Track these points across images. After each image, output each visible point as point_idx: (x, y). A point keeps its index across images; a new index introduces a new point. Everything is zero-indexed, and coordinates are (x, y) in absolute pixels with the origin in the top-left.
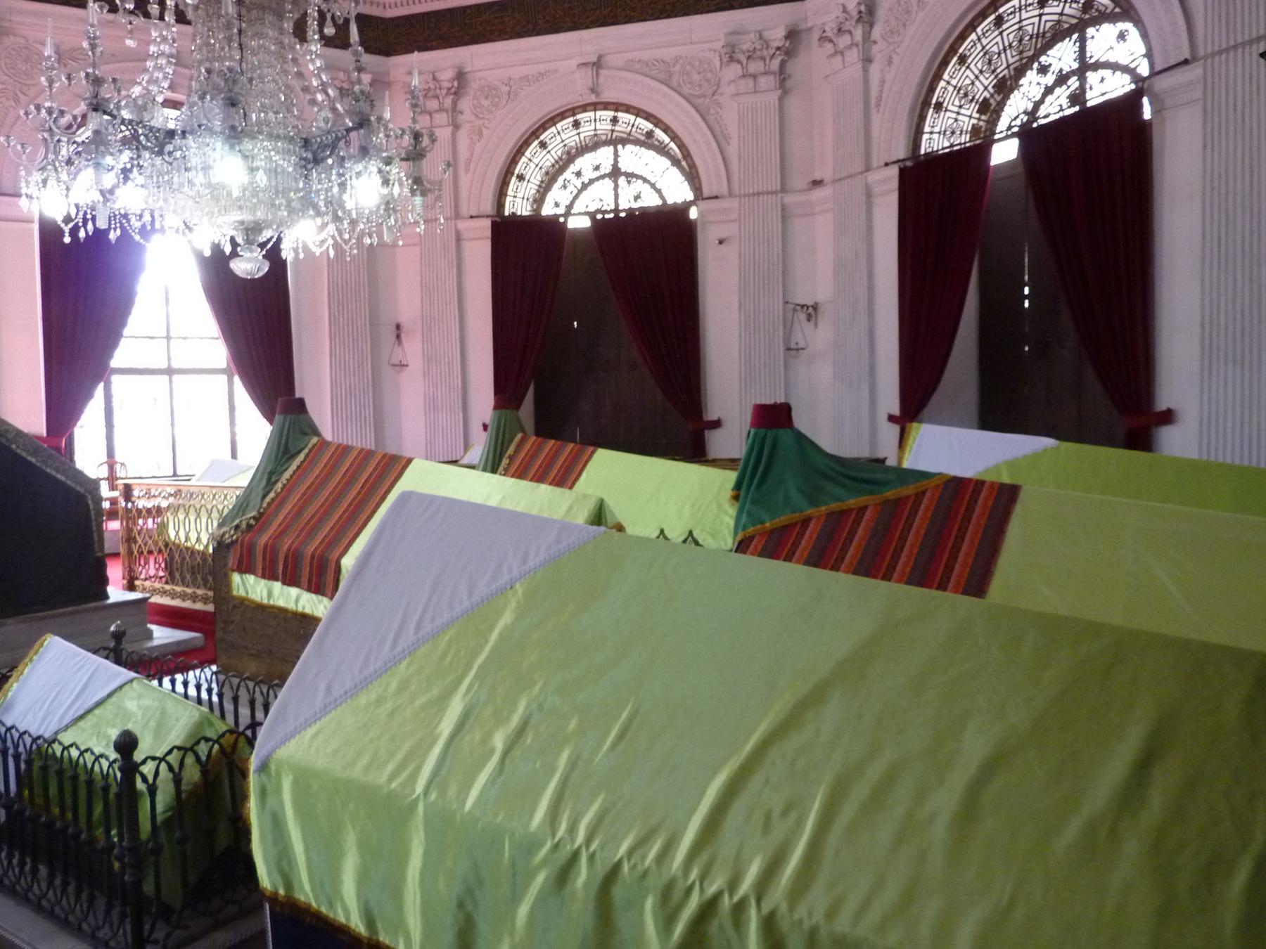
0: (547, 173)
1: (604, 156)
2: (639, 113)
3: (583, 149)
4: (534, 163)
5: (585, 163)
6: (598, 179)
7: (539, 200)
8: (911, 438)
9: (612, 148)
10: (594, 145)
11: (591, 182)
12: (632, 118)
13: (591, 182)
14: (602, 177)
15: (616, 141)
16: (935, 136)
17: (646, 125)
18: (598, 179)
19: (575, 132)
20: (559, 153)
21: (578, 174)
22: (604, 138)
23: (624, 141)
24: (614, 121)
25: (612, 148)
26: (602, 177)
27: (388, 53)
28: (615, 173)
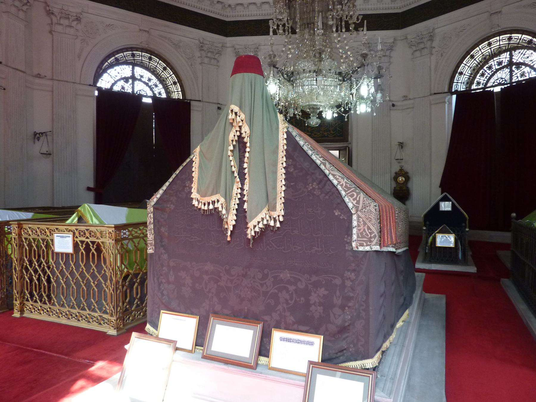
0: (474, 70)
1: (505, 58)
2: (523, 32)
3: (493, 56)
4: (466, 67)
5: (493, 63)
6: (500, 69)
7: (470, 82)
8: (243, 371)
9: (131, 66)
10: (499, 52)
11: (497, 70)
12: (520, 35)
13: (497, 70)
14: (503, 67)
15: (511, 49)
16: (459, 84)
17: (528, 38)
18: (500, 69)
19: (132, 58)
20: (163, 76)
21: (156, 86)
22: (504, 48)
23: (515, 49)
24: (510, 39)
25: (131, 66)
26: (503, 67)
27: (226, 35)
28: (511, 63)
